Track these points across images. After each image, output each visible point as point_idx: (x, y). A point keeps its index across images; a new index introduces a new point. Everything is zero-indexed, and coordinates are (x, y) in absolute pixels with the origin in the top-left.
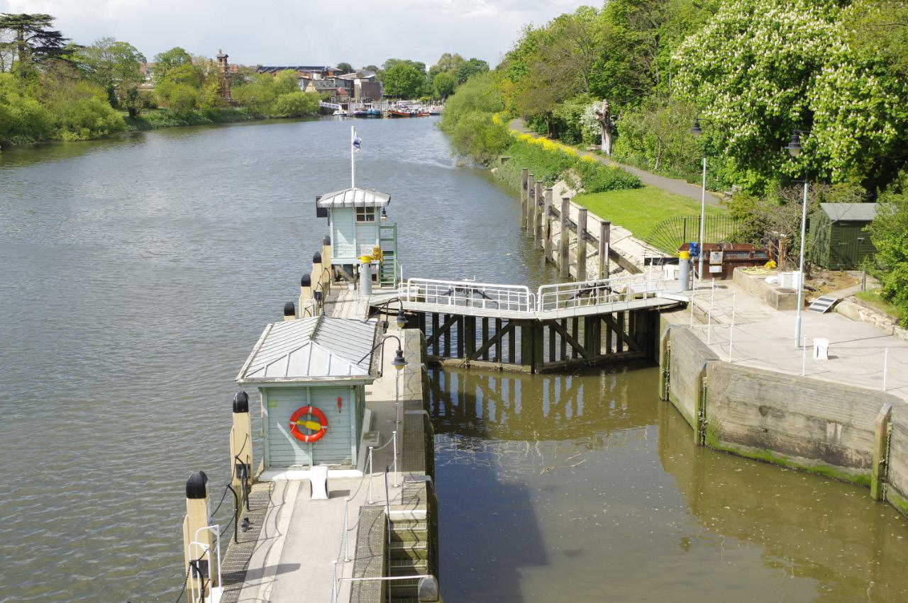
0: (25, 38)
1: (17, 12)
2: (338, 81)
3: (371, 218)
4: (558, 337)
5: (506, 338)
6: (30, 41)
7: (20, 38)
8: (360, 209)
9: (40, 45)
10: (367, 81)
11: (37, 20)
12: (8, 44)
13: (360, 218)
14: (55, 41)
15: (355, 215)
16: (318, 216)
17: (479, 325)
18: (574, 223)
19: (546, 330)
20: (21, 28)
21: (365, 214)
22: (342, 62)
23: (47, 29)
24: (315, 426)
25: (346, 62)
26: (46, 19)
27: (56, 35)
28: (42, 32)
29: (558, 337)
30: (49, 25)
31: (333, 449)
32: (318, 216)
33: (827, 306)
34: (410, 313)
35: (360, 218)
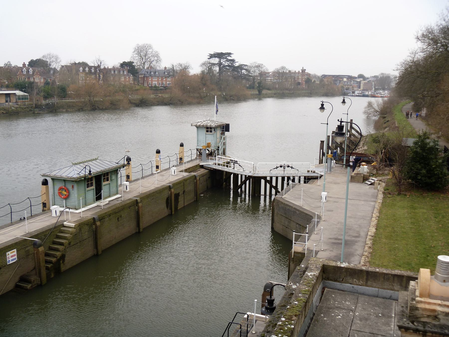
0: (222, 61)
1: (219, 51)
2: (354, 81)
3: (211, 131)
4: (268, 185)
5: (248, 182)
6: (224, 63)
7: (220, 61)
8: (207, 128)
9: (227, 64)
10: (367, 82)
11: (226, 55)
12: (216, 64)
13: (207, 131)
14: (232, 63)
15: (205, 130)
16: (229, 132)
17: (240, 176)
18: (336, 142)
19: (263, 181)
20: (219, 57)
21: (209, 130)
22: (363, 74)
23: (229, 58)
24: (65, 193)
25: (362, 74)
26: (229, 54)
27: (233, 61)
28: (228, 59)
29: (268, 185)
30: (230, 56)
31: (445, 268)
32: (229, 132)
33: (371, 182)
34: (212, 169)
35: (207, 131)
